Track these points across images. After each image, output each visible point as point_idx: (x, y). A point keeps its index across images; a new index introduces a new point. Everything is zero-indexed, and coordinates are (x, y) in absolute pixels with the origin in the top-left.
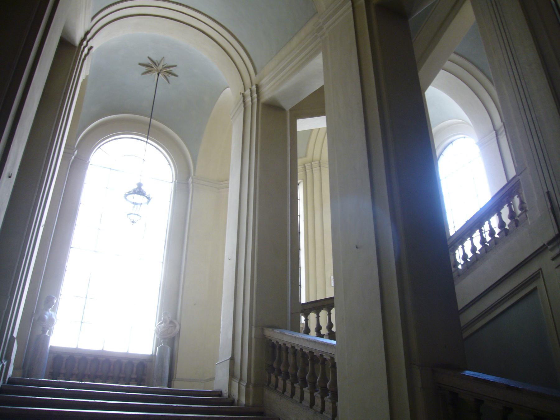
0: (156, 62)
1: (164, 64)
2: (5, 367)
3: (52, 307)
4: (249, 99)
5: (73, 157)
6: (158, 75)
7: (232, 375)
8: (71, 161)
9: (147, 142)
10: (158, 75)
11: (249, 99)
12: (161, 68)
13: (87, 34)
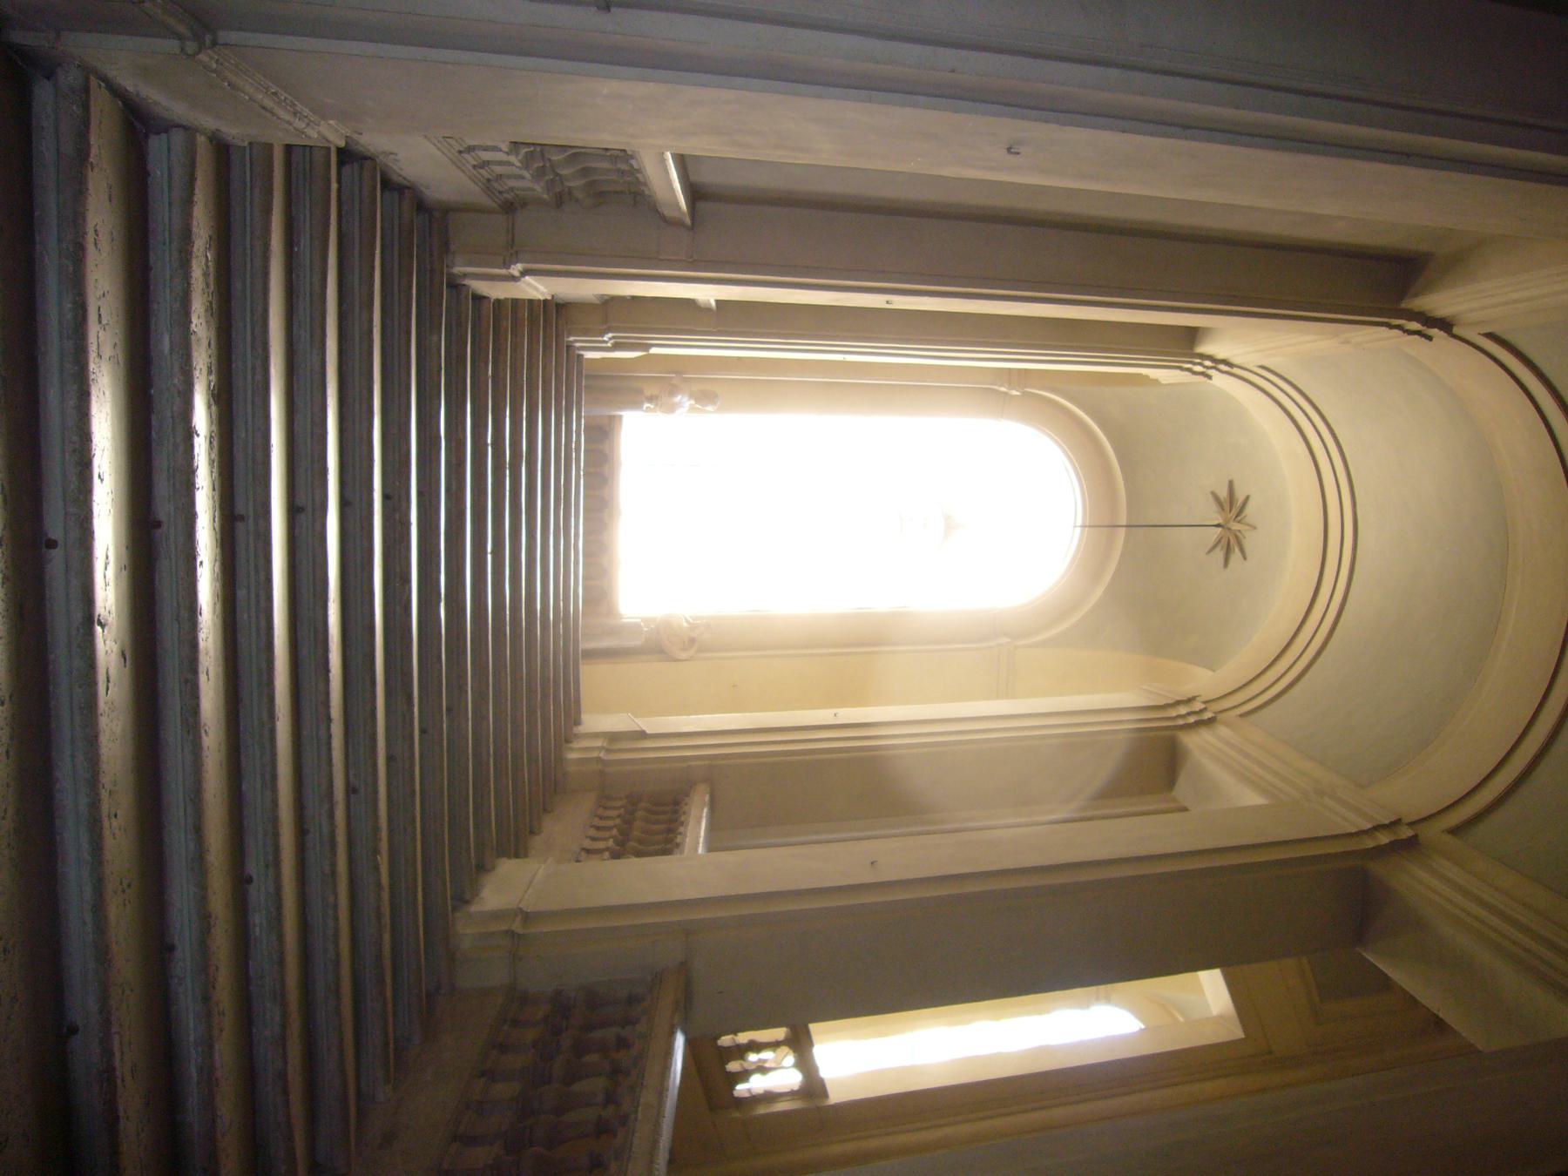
0: (1243, 516)
1: (1243, 532)
2: (604, 345)
3: (697, 406)
4: (1183, 710)
5: (1003, 389)
6: (1218, 526)
7: (614, 737)
8: (996, 387)
9: (1075, 527)
10: (1218, 526)
11: (1183, 710)
12: (1233, 528)
13: (1225, 362)
